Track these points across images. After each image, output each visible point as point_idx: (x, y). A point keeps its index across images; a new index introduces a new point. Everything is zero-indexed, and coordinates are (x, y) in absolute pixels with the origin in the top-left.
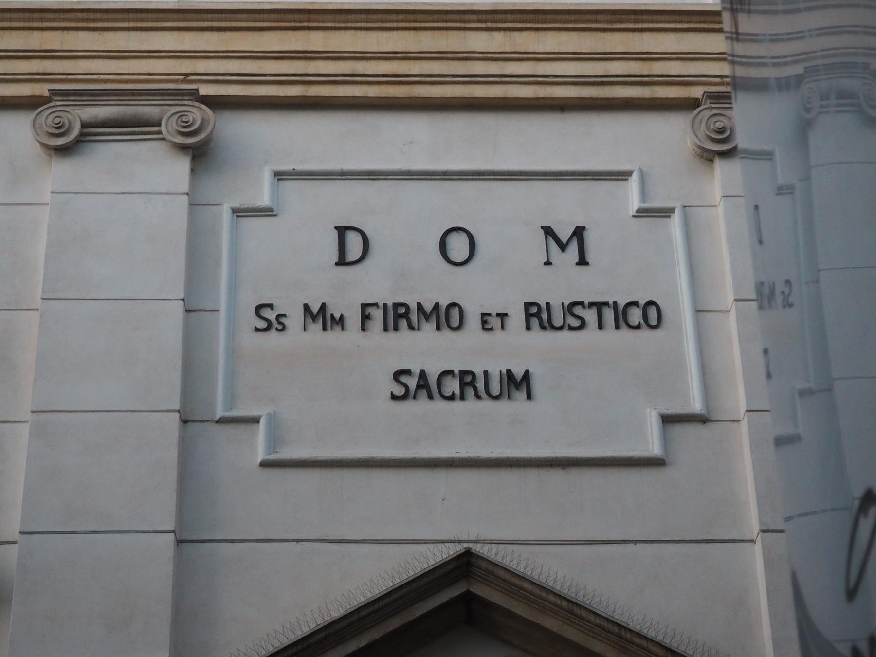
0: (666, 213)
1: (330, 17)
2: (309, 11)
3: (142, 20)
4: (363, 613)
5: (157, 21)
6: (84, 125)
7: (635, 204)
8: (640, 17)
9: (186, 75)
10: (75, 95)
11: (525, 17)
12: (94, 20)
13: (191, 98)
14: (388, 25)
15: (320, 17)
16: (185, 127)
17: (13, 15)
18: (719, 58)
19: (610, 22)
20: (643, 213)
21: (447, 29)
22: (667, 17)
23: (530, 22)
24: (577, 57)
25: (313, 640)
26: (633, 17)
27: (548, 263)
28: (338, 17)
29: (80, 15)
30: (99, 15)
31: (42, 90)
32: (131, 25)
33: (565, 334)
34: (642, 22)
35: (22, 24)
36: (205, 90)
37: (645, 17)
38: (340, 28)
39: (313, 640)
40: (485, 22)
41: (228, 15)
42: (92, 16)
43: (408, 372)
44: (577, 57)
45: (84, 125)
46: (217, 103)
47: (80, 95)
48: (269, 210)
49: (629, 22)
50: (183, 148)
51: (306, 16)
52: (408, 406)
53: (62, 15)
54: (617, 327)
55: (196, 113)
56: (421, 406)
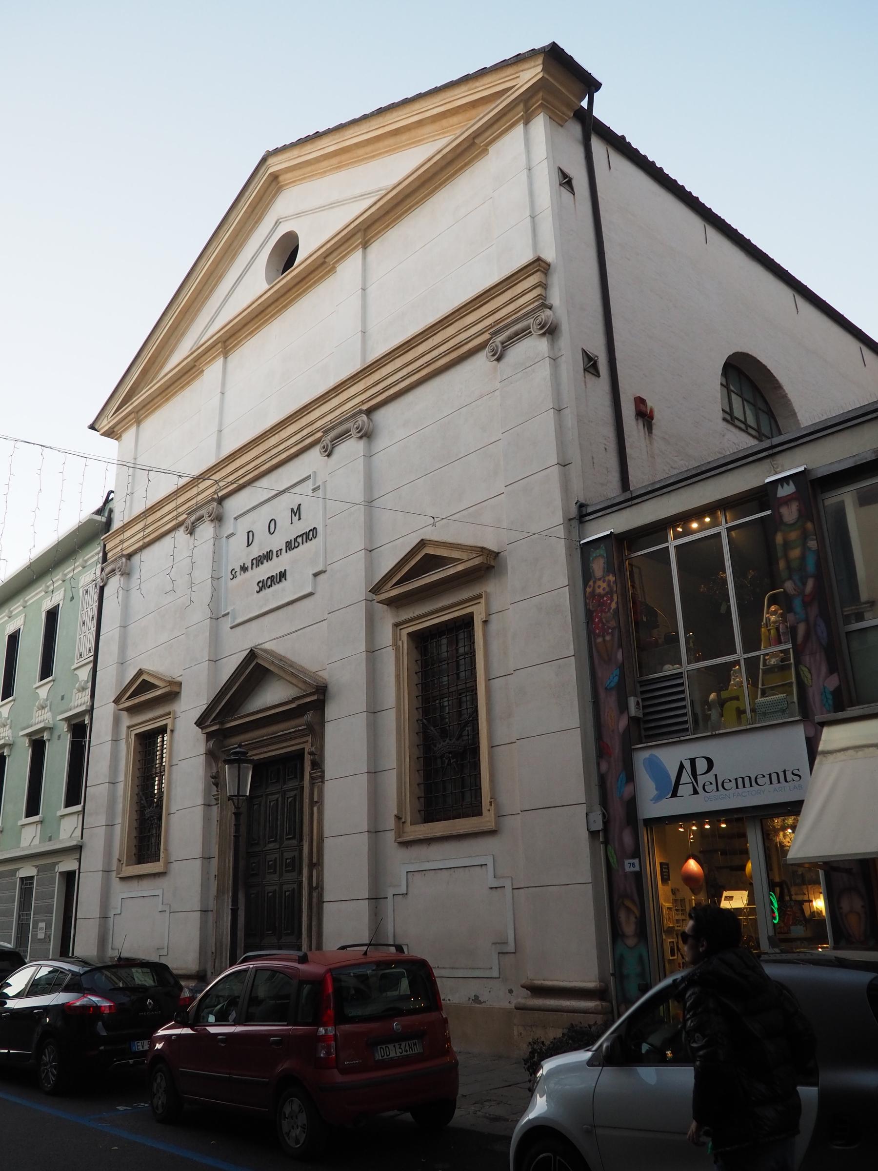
2: (233, 454)
3: (185, 489)
4: (232, 678)
6: (502, 343)
8: (307, 408)
9: (362, 402)
13: (541, 308)
14: (251, 447)
15: (414, 341)
16: (493, 351)
18: (211, 486)
19: (301, 414)
21: (264, 441)
22: (313, 404)
24: (295, 433)
25: (223, 690)
26: (305, 409)
27: (292, 523)
31: (486, 336)
34: (308, 409)
39: (223, 690)
40: (272, 433)
44: (295, 433)
45: (502, 343)
48: (233, 533)
49: (305, 411)
50: (544, 334)
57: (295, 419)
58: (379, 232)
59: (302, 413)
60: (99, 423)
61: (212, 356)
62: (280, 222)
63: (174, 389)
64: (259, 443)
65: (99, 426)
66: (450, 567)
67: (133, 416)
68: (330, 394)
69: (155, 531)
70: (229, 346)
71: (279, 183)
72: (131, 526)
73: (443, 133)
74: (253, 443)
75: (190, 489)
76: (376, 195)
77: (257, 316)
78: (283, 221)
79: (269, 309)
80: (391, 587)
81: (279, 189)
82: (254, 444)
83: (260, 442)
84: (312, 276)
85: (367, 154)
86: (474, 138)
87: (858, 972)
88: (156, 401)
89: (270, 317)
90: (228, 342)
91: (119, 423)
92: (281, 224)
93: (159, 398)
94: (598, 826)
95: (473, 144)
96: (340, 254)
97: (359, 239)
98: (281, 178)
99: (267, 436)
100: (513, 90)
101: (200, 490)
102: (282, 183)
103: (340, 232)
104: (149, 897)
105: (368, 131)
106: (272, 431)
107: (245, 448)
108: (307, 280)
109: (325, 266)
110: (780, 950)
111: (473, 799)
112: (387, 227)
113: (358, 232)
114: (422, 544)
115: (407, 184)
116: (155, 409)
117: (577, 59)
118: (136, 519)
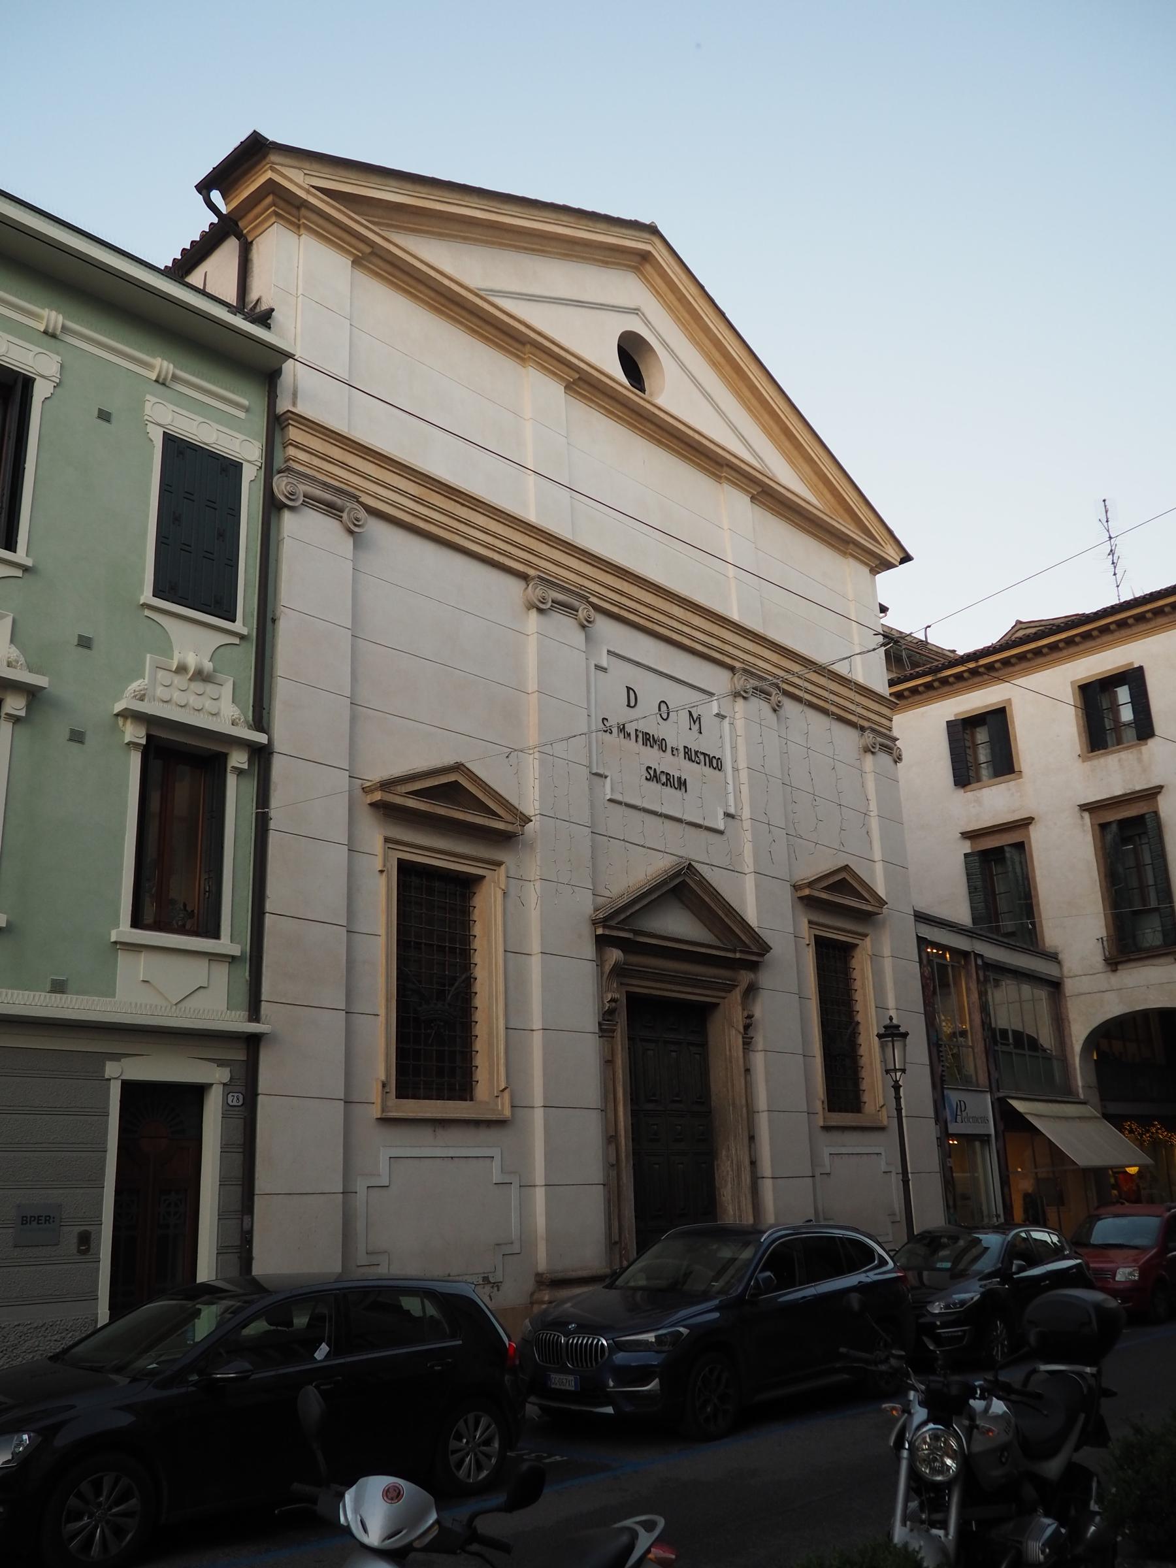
0: (724, 717)
1: (633, 577)
2: (627, 572)
5: (572, 551)
7: (715, 711)
10: (546, 581)
11: (692, 605)
12: (550, 541)
16: (290, 494)
17: (522, 524)
20: (718, 715)
23: (488, 512)
27: (690, 729)
28: (636, 579)
29: (547, 536)
30: (553, 539)
32: (563, 549)
33: (695, 764)
35: (523, 530)
36: (593, 599)
37: (727, 622)
38: (865, 696)
40: (680, 602)
41: (373, 453)
42: (551, 538)
43: (651, 768)
46: (598, 609)
47: (548, 582)
48: (606, 669)
51: (624, 573)
52: (650, 783)
53: (540, 533)
54: (710, 767)
55: (362, 514)
56: (653, 785)
57: (709, 618)
58: (764, 504)
59: (719, 621)
60: (288, 161)
61: (555, 370)
62: (637, 314)
63: (463, 318)
64: (683, 606)
65: (282, 165)
66: (470, 813)
67: (368, 250)
68: (750, 634)
69: (679, 633)
70: (577, 386)
71: (641, 265)
72: (383, 465)
73: (811, 486)
74: (655, 588)
75: (332, 443)
76: (763, 467)
77: (633, 411)
78: (641, 317)
79: (649, 425)
80: (406, 793)
81: (637, 270)
82: (655, 590)
83: (685, 607)
84: (703, 458)
85: (749, 401)
86: (728, 465)
87: (852, 1285)
88: (422, 288)
89: (639, 429)
90: (581, 383)
91: (358, 238)
92: (635, 316)
93: (432, 294)
94: (613, 1160)
95: (721, 465)
96: (737, 479)
97: (755, 490)
98: (648, 268)
99: (674, 599)
100: (876, 545)
101: (806, 676)
102: (642, 268)
103: (680, 421)
104: (465, 1159)
105: (773, 397)
106: (682, 601)
107: (643, 582)
108: (697, 455)
109: (294, 211)
110: (231, 1313)
111: (668, 1112)
112: (473, 332)
113: (760, 486)
114: (458, 767)
115: (453, 288)
116: (410, 293)
117: (216, 162)
118: (408, 470)
